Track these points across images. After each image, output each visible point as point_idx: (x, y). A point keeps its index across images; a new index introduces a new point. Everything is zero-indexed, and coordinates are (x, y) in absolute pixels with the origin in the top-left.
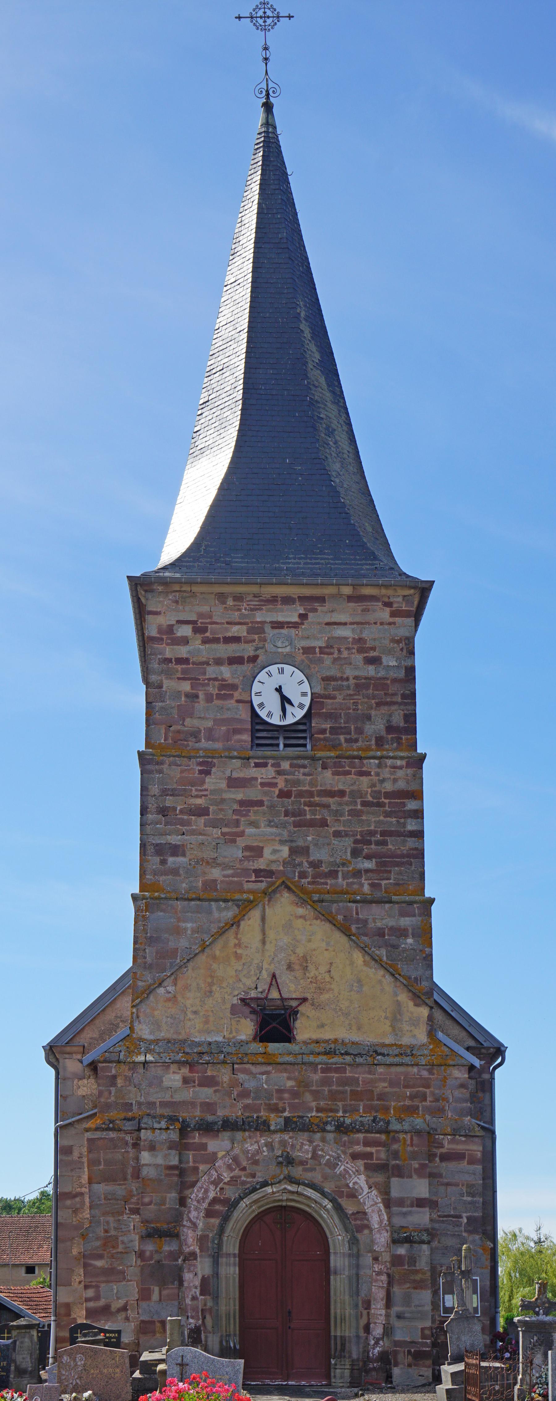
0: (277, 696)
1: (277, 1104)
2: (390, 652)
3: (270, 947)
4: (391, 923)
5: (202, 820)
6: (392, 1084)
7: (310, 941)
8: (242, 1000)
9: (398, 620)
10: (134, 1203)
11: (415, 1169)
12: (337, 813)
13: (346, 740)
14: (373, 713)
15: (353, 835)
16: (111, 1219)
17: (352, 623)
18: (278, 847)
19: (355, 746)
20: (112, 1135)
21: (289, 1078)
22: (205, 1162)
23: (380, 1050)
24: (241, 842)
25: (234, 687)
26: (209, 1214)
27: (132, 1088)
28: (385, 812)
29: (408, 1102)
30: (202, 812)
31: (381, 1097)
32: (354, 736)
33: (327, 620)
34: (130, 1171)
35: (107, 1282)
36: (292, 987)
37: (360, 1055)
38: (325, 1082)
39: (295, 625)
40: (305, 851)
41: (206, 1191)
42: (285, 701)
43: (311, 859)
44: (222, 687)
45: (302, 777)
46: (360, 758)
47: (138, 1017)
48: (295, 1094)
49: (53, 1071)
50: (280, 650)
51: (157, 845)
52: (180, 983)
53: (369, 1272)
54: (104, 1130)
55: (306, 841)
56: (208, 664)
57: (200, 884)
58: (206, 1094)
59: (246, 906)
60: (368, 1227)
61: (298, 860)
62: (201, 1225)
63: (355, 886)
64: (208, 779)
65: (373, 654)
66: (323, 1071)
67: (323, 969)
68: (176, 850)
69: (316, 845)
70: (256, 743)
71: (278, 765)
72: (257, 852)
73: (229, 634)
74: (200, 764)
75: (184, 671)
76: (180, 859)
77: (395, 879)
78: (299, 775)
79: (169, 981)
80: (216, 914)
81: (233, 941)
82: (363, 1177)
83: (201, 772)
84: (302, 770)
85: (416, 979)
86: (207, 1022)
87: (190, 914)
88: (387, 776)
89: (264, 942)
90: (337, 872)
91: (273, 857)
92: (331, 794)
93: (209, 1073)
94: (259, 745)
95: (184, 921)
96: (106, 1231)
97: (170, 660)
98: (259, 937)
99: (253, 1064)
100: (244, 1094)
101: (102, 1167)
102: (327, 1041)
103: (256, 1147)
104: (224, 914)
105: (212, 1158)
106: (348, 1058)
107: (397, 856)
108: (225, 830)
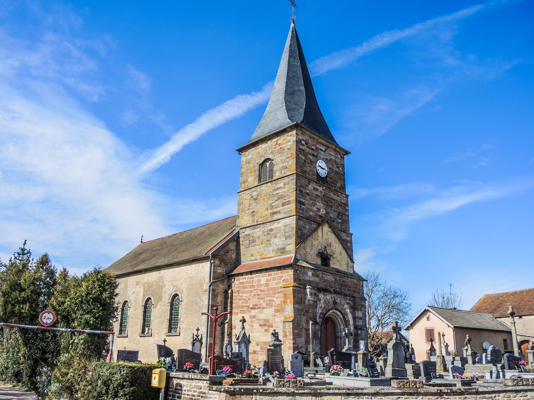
1: (331, 285)
3: (324, 238)
12: (334, 205)
30: (308, 195)
35: (298, 338)
38: (340, 280)
41: (319, 311)
58: (317, 279)
78: (327, 192)
89: (322, 236)
96: (298, 321)
98: (321, 235)
99: (326, 272)
100: (325, 281)
104: (314, 226)
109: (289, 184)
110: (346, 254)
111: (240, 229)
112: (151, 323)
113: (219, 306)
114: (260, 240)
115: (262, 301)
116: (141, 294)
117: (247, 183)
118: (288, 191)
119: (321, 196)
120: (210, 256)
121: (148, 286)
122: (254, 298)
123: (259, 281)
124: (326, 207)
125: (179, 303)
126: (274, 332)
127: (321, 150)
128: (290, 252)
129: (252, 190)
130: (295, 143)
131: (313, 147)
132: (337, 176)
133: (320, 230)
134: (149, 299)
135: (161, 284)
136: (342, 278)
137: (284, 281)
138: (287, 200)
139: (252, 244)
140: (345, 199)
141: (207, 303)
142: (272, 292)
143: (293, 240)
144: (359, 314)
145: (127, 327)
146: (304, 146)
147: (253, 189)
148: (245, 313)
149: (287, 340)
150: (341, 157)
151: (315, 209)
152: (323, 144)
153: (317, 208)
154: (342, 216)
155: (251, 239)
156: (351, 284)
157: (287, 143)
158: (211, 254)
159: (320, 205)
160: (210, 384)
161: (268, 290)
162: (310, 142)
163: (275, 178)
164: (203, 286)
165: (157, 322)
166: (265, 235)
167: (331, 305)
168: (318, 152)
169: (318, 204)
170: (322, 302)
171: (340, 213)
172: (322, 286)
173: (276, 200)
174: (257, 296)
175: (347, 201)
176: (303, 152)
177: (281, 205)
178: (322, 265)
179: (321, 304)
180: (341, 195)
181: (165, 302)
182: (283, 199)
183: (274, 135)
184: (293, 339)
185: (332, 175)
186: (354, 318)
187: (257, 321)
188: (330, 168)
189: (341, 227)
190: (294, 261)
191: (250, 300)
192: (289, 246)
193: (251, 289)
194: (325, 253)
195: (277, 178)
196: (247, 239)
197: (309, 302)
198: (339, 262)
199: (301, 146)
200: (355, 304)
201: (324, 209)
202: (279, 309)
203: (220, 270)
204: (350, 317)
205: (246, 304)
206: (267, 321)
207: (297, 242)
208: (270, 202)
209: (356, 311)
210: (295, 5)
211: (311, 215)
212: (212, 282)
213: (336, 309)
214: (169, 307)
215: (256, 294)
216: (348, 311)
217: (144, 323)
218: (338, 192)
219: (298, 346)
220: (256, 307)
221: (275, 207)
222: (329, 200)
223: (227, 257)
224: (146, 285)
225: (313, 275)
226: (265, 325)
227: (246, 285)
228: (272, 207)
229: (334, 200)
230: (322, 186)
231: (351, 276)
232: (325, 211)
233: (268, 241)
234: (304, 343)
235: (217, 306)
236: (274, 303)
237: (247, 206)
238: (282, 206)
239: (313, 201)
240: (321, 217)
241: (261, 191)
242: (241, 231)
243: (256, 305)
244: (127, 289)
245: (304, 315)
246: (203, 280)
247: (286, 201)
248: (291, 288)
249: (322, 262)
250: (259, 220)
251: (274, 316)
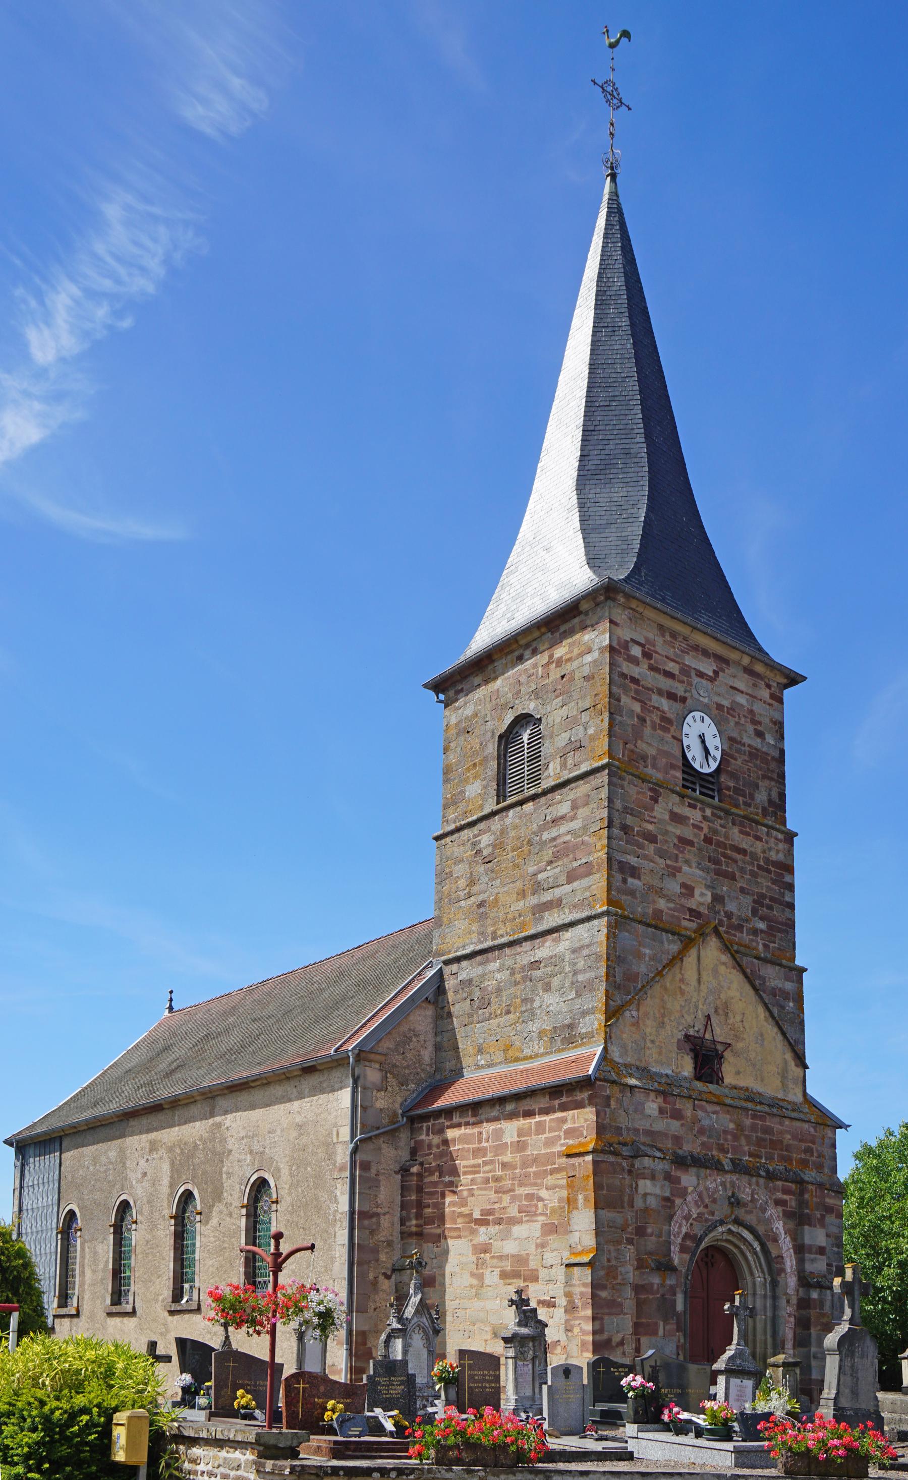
1: (723, 1145)
3: (703, 987)
10: (629, 1233)
12: (742, 870)
15: (753, 895)
16: (612, 1248)
17: (747, 694)
20: (612, 1159)
21: (731, 1121)
22: (680, 1197)
28: (772, 879)
30: (652, 839)
33: (731, 684)
34: (626, 1199)
35: (609, 1314)
37: (761, 1103)
38: (754, 1128)
41: (680, 1226)
43: (726, 909)
47: (610, 1038)
49: (808, 1091)
50: (701, 699)
52: (642, 1010)
55: (722, 890)
56: (652, 690)
57: (650, 911)
58: (675, 1126)
59: (688, 943)
67: (738, 1018)
69: (729, 896)
76: (636, 882)
77: (779, 944)
78: (717, 825)
79: (634, 1007)
81: (679, 976)
84: (719, 821)
87: (647, 940)
89: (699, 981)
90: (743, 926)
93: (677, 1106)
95: (644, 947)
96: (609, 1261)
98: (696, 977)
99: (707, 1102)
100: (702, 1131)
101: (605, 1192)
104: (671, 946)
108: (668, 862)
109: (587, 804)
110: (779, 1037)
111: (447, 963)
112: (197, 1269)
113: (385, 1214)
114: (504, 998)
115: (506, 1199)
116: (166, 1181)
117: (464, 803)
118: (585, 828)
119: (695, 840)
120: (349, 1057)
121: (182, 1153)
122: (485, 1189)
123: (499, 1134)
124: (713, 880)
125: (270, 1207)
126: (515, 1297)
127: (701, 675)
128: (590, 1035)
129: (475, 830)
130: (607, 655)
131: (672, 664)
132: (756, 766)
133: (690, 959)
134: (188, 1196)
135: (219, 1148)
136: (762, 1118)
137: (569, 1133)
138: (584, 861)
139: (480, 1012)
140: (781, 846)
141: (346, 1208)
142: (534, 1169)
143: (597, 999)
144: (816, 1236)
145: (132, 1282)
146: (638, 664)
147: (482, 826)
148: (459, 1237)
149: (577, 1322)
150: (772, 696)
151: (673, 887)
152: (706, 653)
153: (684, 885)
154: (770, 908)
155: (477, 994)
156: (794, 1137)
157: (581, 655)
158: (354, 1048)
159: (692, 872)
160: (260, 1456)
161: (525, 1164)
162: (660, 646)
163: (546, 784)
164: (334, 1153)
165: (212, 1266)
166: (516, 983)
167: (722, 1210)
168: (690, 684)
169: (685, 868)
170: (689, 1198)
171: (763, 896)
172: (691, 1146)
173: (550, 863)
174: (492, 1184)
175: (790, 853)
176: (633, 686)
177: (563, 879)
178: (698, 1077)
179: (689, 1207)
180: (768, 834)
181: (231, 1204)
182: (571, 856)
183: (543, 630)
184: (594, 1319)
185: (739, 762)
186: (800, 1249)
187: (495, 1261)
188: (731, 739)
189: (765, 946)
190: (598, 1068)
191: (473, 1195)
192: (587, 1018)
193: (477, 1161)
194: (708, 1036)
195: (551, 783)
196: (465, 995)
197: (645, 1201)
198: (754, 1065)
199: (627, 668)
200: (802, 1203)
201: (707, 887)
202: (556, 1222)
203: (382, 1102)
204: (786, 1246)
205: (462, 1209)
206: (521, 1260)
207: (611, 1003)
208: (531, 869)
209: (806, 1227)
210: (620, 101)
211: (661, 911)
212: (361, 1140)
213: (738, 1222)
214: (244, 1220)
215: (490, 1175)
216: (779, 1226)
217: (179, 1268)
218: (757, 823)
219: (609, 1341)
220: (491, 1218)
221: (545, 886)
222: (725, 856)
223: (403, 1059)
224: (178, 1151)
225: (661, 1111)
226: (516, 1275)
227: (460, 1147)
228: (538, 887)
229: (743, 852)
230: (699, 805)
231: (793, 1110)
232: (709, 894)
233: (525, 1001)
234: (631, 1330)
235: (377, 1215)
236: (540, 1204)
237: (462, 883)
238: (568, 883)
239: (668, 862)
240: (694, 914)
241: (503, 832)
242: (447, 970)
243: (490, 1212)
244: (124, 1164)
245: (630, 1241)
246: (335, 1133)
247: (579, 862)
248: (589, 1158)
249: (695, 1068)
250: (499, 932)
251: (542, 1246)
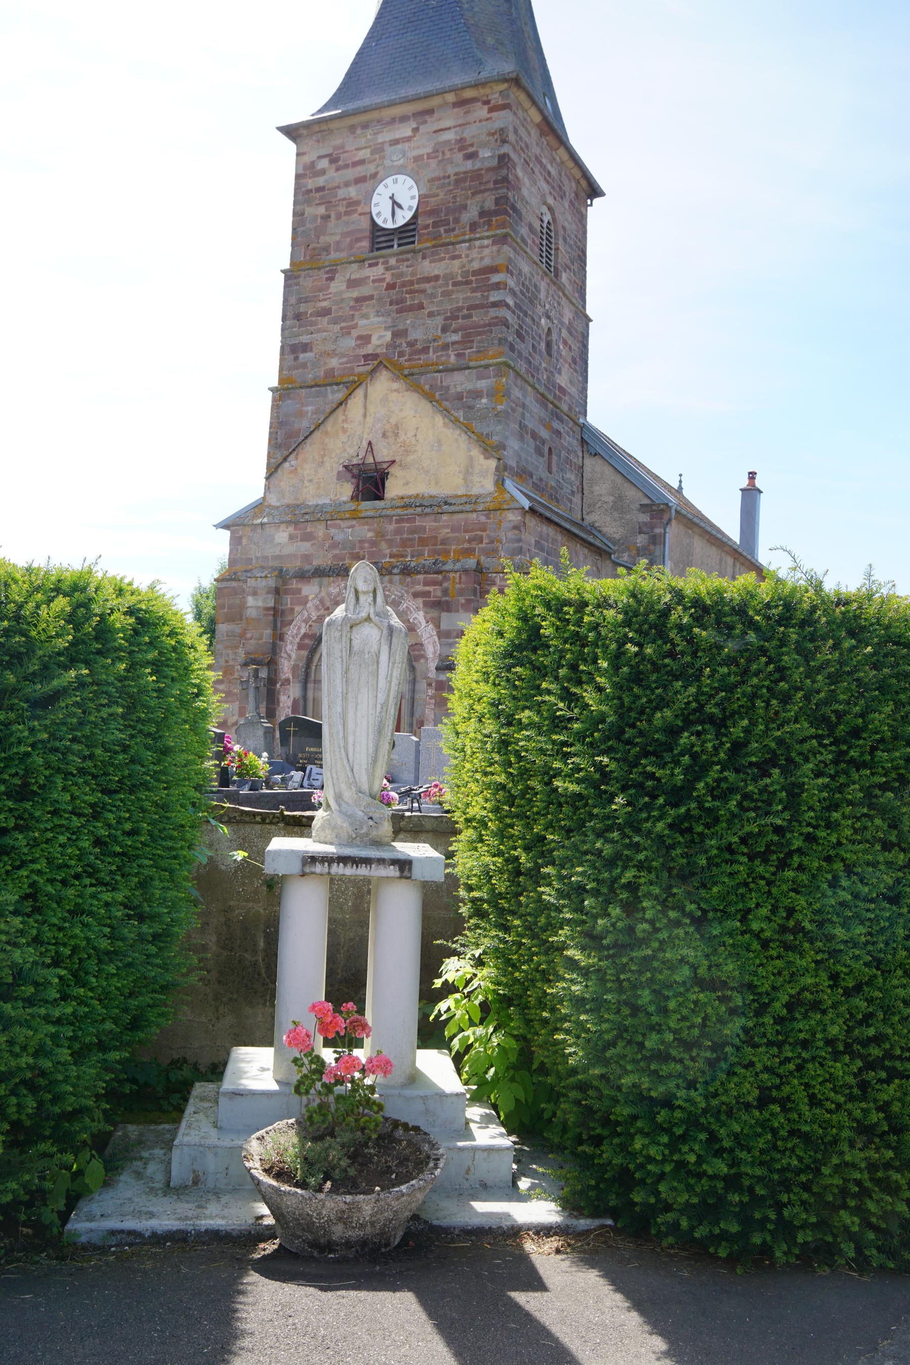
0: (390, 202)
2: (484, 145)
3: (370, 420)
4: (469, 386)
5: (326, 319)
6: (453, 530)
7: (401, 410)
8: (346, 467)
9: (495, 114)
11: (462, 605)
13: (446, 231)
14: (469, 202)
16: (230, 652)
18: (383, 333)
19: (452, 234)
20: (234, 584)
21: (369, 530)
22: (300, 604)
23: (450, 501)
24: (355, 333)
25: (358, 203)
26: (300, 647)
27: (253, 547)
29: (466, 545)
30: (326, 312)
31: (444, 542)
32: (452, 226)
33: (435, 128)
36: (385, 452)
38: (398, 532)
39: (408, 139)
40: (402, 333)
41: (299, 628)
42: (396, 204)
44: (349, 204)
45: (405, 269)
46: (452, 244)
48: (373, 543)
51: (292, 345)
53: (424, 696)
54: (228, 580)
59: (353, 386)
60: (423, 656)
61: (398, 342)
62: (294, 656)
63: (444, 358)
64: (332, 284)
65: (471, 150)
66: (398, 522)
67: (410, 434)
68: (306, 348)
69: (413, 326)
70: (375, 246)
71: (387, 262)
72: (365, 339)
73: (357, 159)
74: (327, 272)
75: (321, 198)
80: (330, 397)
82: (421, 613)
83: (327, 279)
85: (487, 435)
86: (318, 488)
88: (475, 255)
89: (365, 416)
91: (379, 342)
92: (428, 280)
94: (378, 249)
96: (227, 662)
97: (311, 191)
98: (362, 411)
100: (334, 545)
102: (410, 497)
103: (337, 590)
105: (304, 602)
106: (419, 509)
107: (480, 327)
108: (343, 325)
170: (309, 605)
